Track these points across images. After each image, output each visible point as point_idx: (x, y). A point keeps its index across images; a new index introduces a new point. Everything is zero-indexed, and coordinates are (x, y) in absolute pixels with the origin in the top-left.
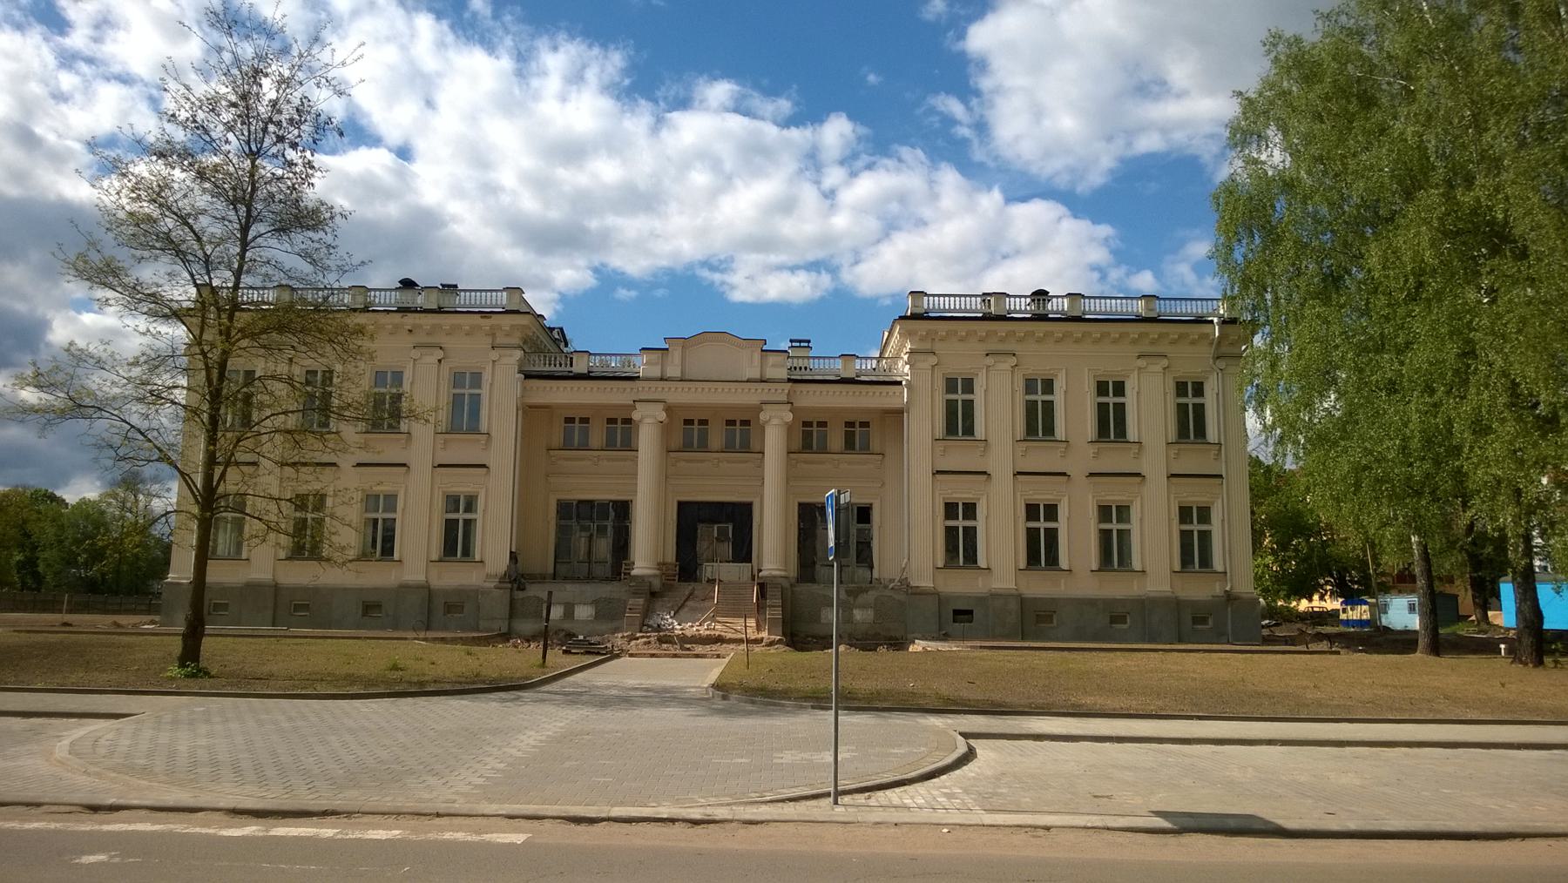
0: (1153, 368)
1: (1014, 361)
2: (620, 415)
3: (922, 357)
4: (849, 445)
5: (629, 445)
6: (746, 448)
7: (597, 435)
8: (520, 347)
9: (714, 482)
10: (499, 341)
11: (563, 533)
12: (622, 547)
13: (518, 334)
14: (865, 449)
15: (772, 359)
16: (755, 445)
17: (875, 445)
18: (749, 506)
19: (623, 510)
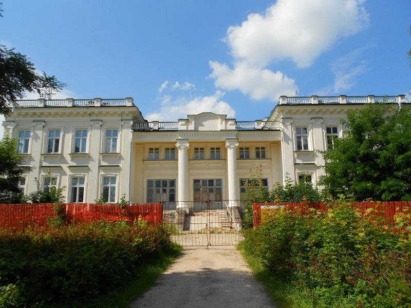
0: (317, 123)
1: (322, 121)
2: (170, 146)
3: (287, 120)
4: (258, 156)
5: (175, 158)
6: (219, 158)
7: (162, 154)
8: (132, 120)
9: (207, 172)
10: (124, 118)
11: (150, 192)
12: (173, 198)
13: (131, 115)
14: (264, 157)
15: (230, 122)
16: (222, 156)
17: (267, 155)
18: (219, 181)
19: (173, 183)
